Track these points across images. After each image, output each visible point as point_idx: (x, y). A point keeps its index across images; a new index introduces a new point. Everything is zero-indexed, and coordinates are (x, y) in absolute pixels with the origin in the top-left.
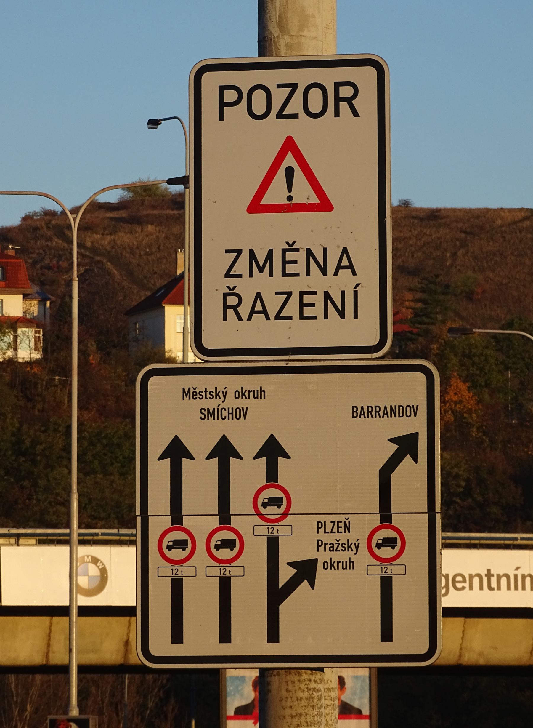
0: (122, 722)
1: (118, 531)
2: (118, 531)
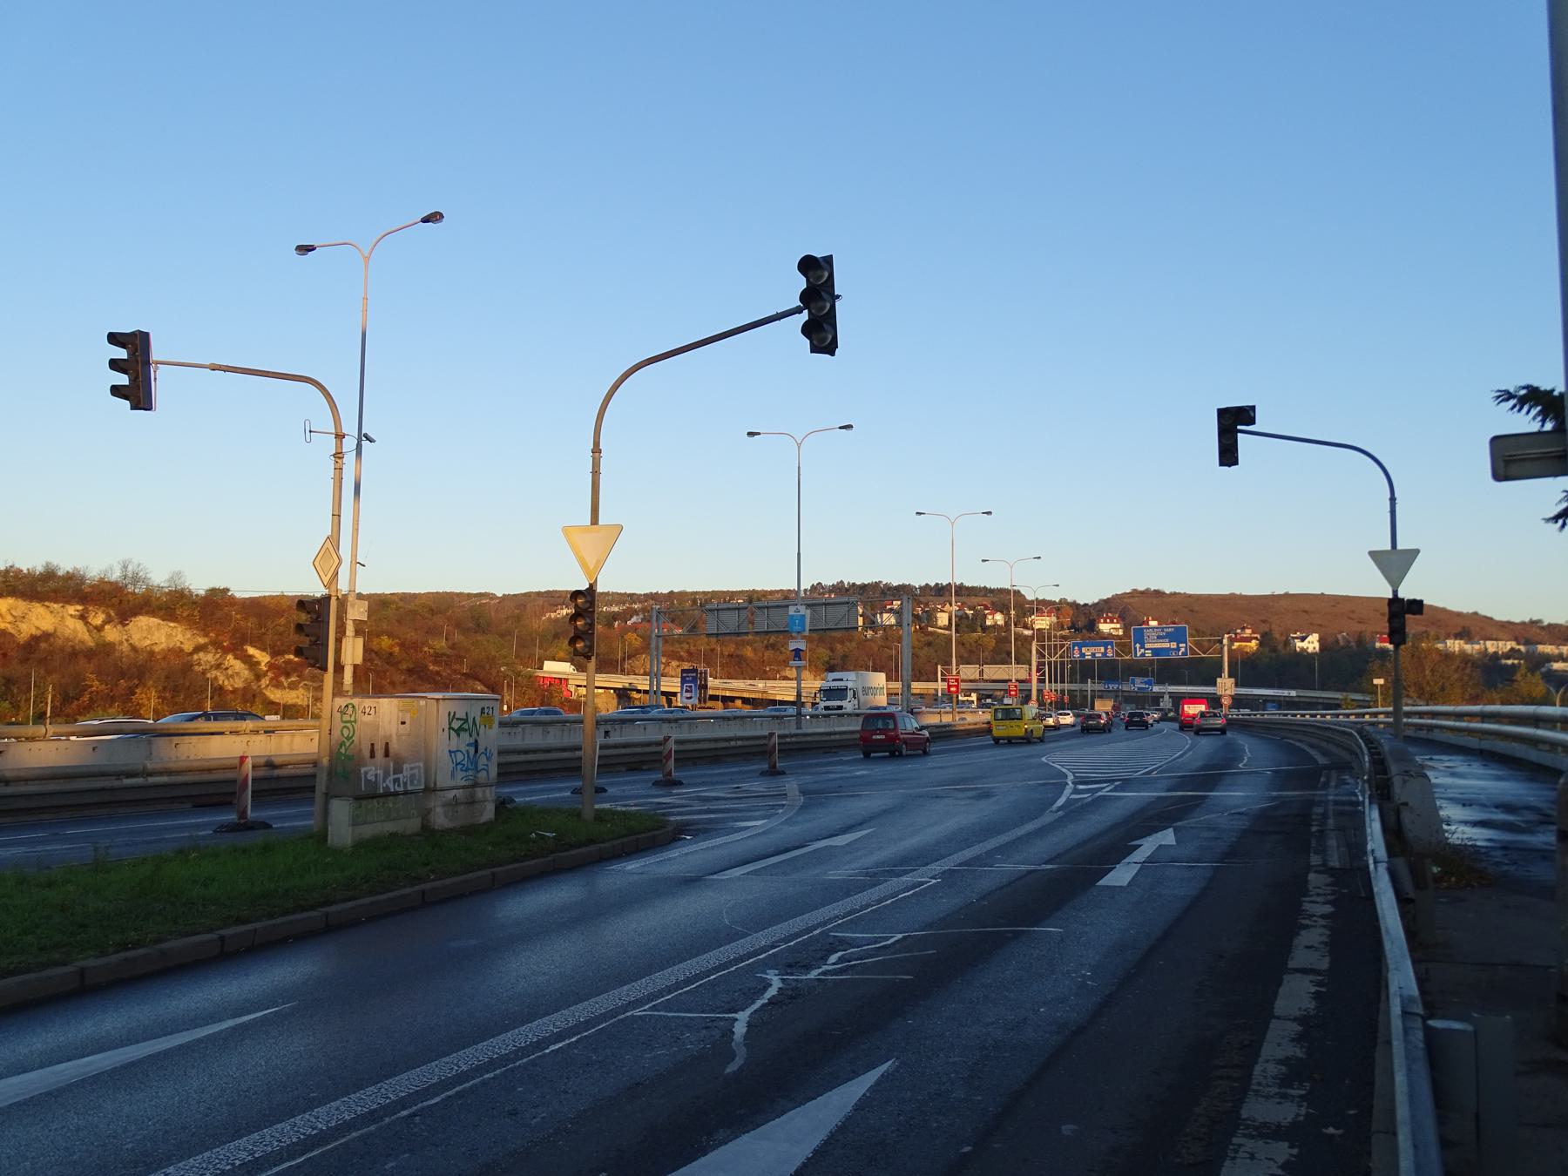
0: (1522, 648)
1: (981, 673)
2: (981, 673)
